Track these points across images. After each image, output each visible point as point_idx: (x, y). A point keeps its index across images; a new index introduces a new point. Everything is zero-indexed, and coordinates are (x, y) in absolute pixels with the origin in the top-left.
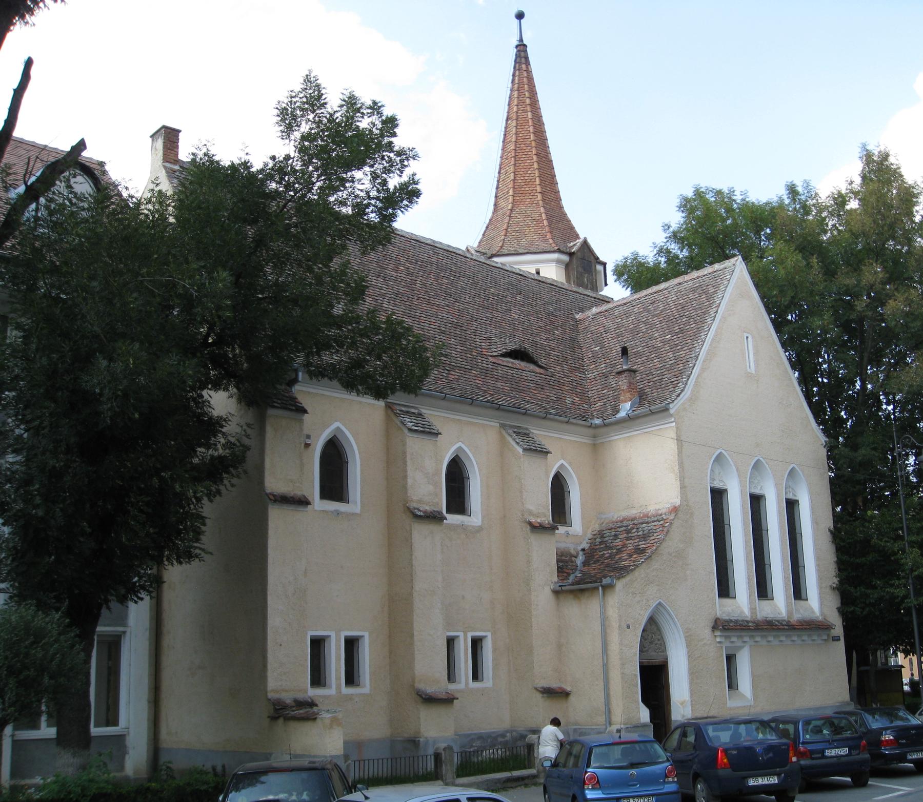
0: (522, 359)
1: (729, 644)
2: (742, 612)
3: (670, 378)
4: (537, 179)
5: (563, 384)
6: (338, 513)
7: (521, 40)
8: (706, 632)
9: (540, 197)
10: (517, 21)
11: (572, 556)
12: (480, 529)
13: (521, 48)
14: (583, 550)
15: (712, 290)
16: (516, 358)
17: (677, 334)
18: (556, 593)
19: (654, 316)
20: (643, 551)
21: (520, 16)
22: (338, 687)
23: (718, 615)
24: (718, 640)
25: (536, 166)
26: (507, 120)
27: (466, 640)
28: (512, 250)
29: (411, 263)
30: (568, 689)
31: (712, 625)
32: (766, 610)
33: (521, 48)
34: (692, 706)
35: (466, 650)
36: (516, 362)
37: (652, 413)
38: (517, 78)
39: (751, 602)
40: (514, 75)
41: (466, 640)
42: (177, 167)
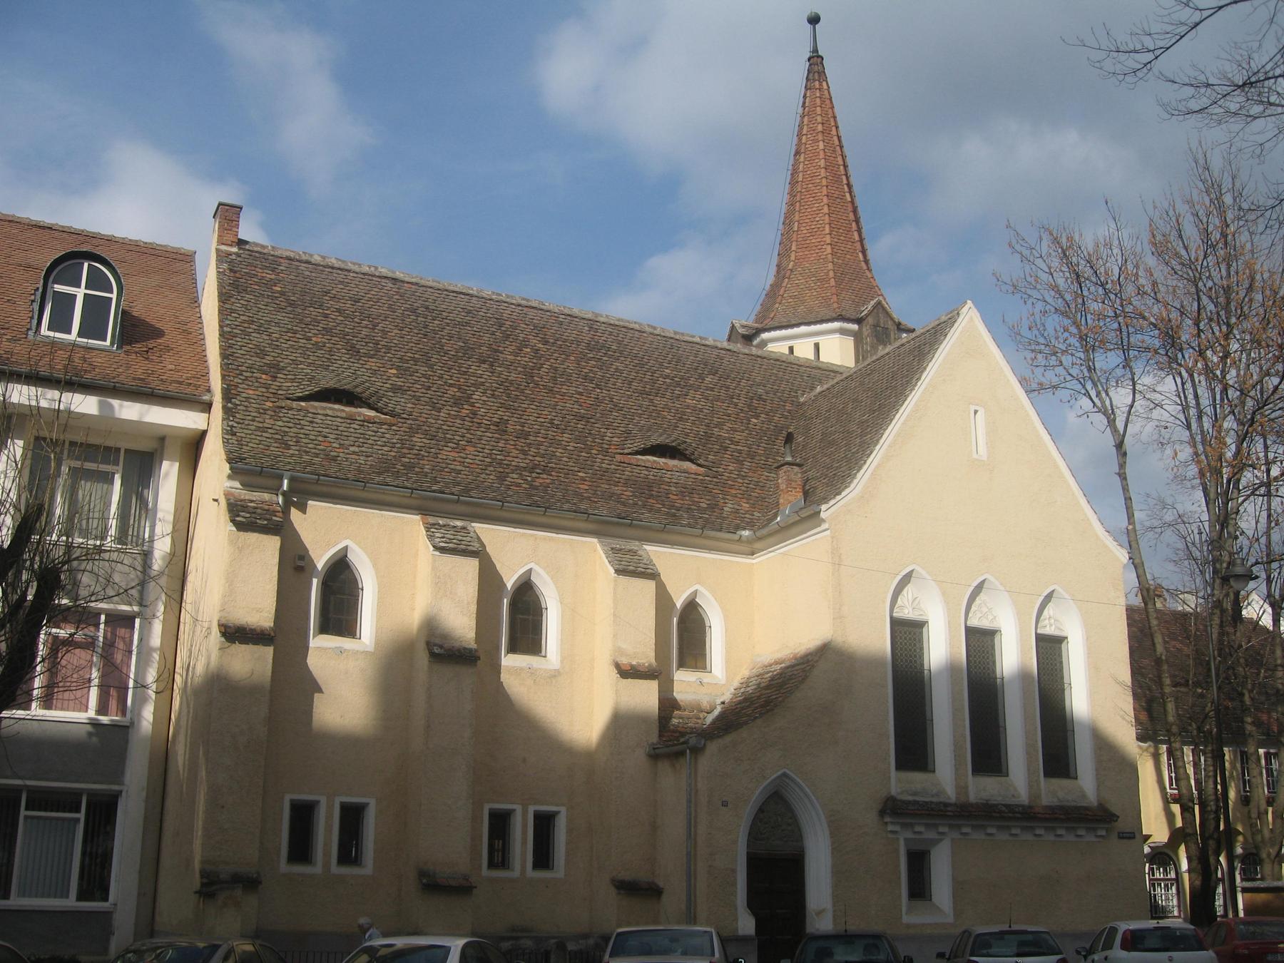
0: (673, 457)
1: (910, 835)
2: (1084, 796)
5: (731, 487)
6: (341, 651)
7: (815, 50)
9: (829, 249)
12: (555, 674)
13: (816, 60)
16: (662, 455)
21: (814, 20)
22: (327, 865)
23: (893, 792)
24: (890, 828)
25: (826, 210)
26: (797, 153)
27: (525, 813)
28: (784, 321)
29: (546, 343)
32: (985, 788)
33: (816, 60)
35: (525, 826)
40: (805, 97)
41: (525, 813)
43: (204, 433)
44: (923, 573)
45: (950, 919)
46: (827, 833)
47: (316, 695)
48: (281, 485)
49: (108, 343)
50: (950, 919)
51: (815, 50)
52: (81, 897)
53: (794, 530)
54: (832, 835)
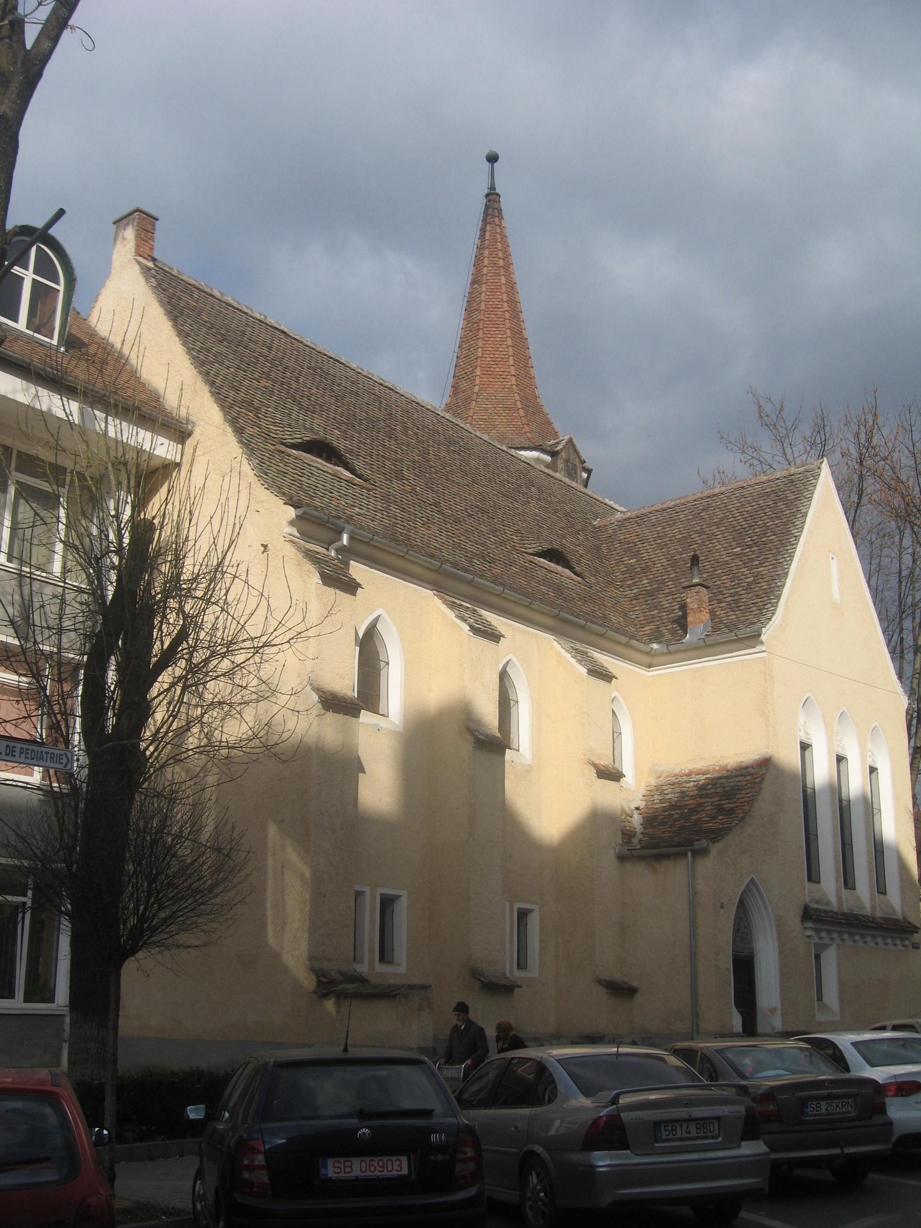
2: (863, 908)
3: (750, 599)
4: (511, 359)
7: (492, 187)
8: (794, 921)
10: (487, 165)
11: (628, 815)
13: (492, 197)
14: (637, 809)
15: (792, 497)
17: (749, 547)
18: (621, 858)
19: (710, 526)
20: (731, 811)
21: (492, 159)
22: (371, 963)
23: (807, 902)
24: (809, 933)
30: (635, 984)
31: (801, 913)
33: (492, 197)
34: (783, 1014)
36: (551, 564)
37: (739, 640)
38: (487, 234)
39: (838, 890)
42: (151, 264)
43: (178, 465)
44: (623, 703)
45: (838, 1019)
46: (775, 936)
47: (360, 774)
48: (340, 538)
49: (55, 342)
50: (838, 1019)
51: (492, 187)
52: (26, 1000)
53: (717, 649)
54: (779, 939)
